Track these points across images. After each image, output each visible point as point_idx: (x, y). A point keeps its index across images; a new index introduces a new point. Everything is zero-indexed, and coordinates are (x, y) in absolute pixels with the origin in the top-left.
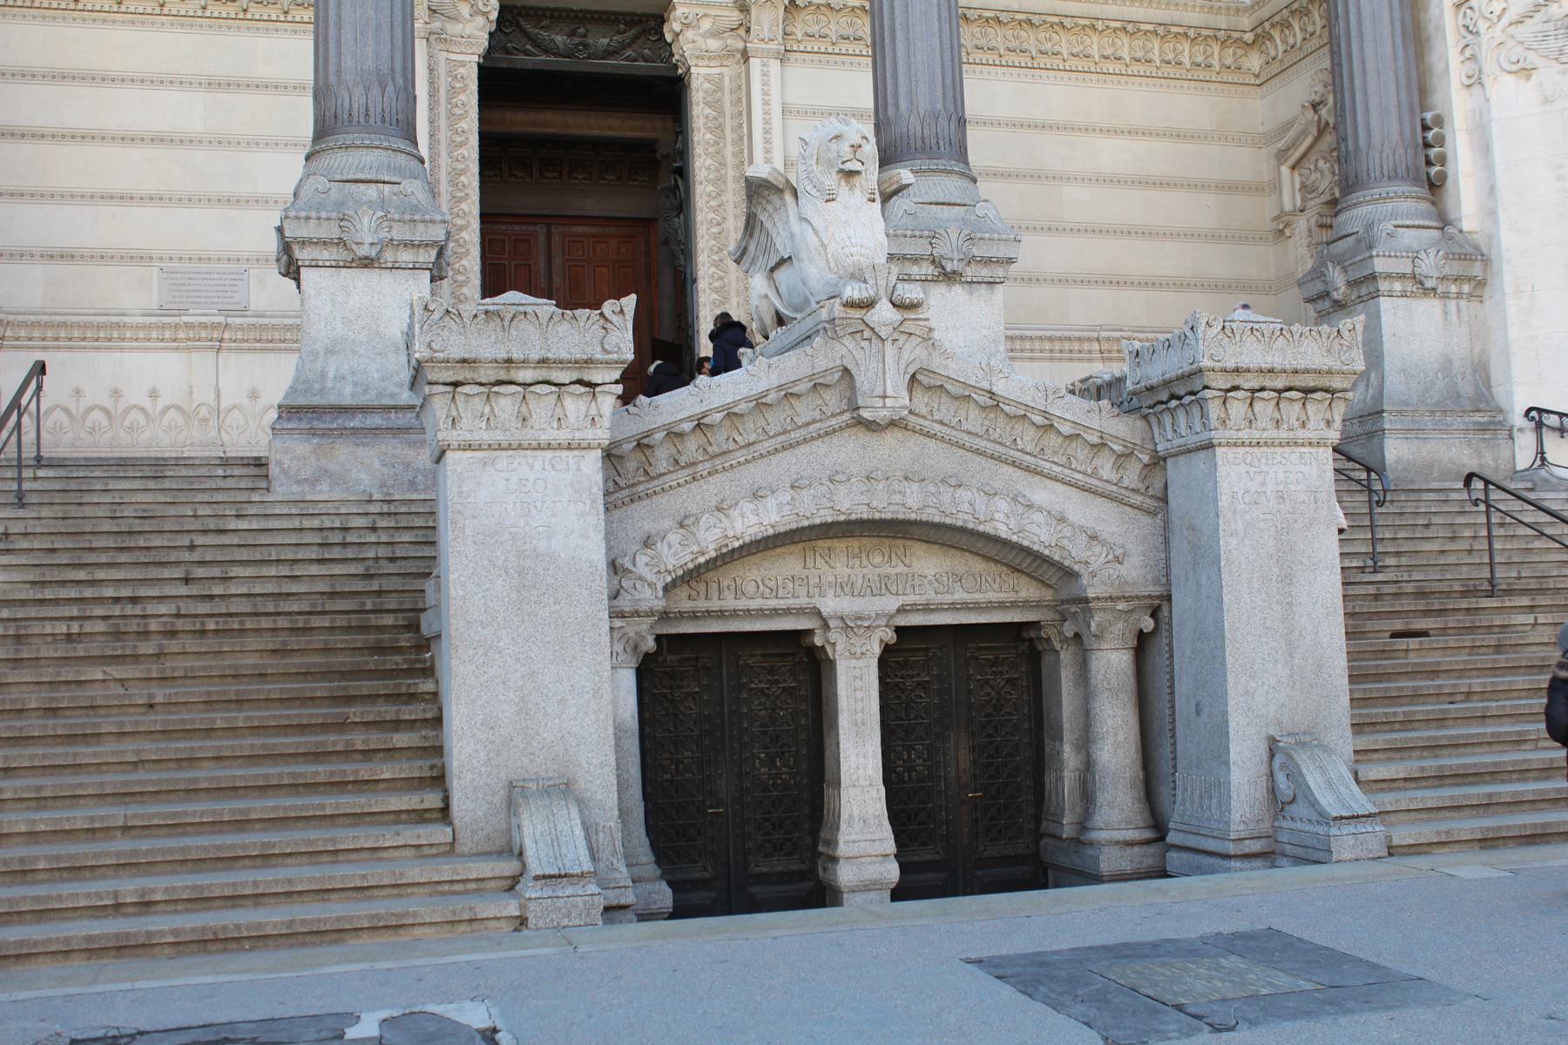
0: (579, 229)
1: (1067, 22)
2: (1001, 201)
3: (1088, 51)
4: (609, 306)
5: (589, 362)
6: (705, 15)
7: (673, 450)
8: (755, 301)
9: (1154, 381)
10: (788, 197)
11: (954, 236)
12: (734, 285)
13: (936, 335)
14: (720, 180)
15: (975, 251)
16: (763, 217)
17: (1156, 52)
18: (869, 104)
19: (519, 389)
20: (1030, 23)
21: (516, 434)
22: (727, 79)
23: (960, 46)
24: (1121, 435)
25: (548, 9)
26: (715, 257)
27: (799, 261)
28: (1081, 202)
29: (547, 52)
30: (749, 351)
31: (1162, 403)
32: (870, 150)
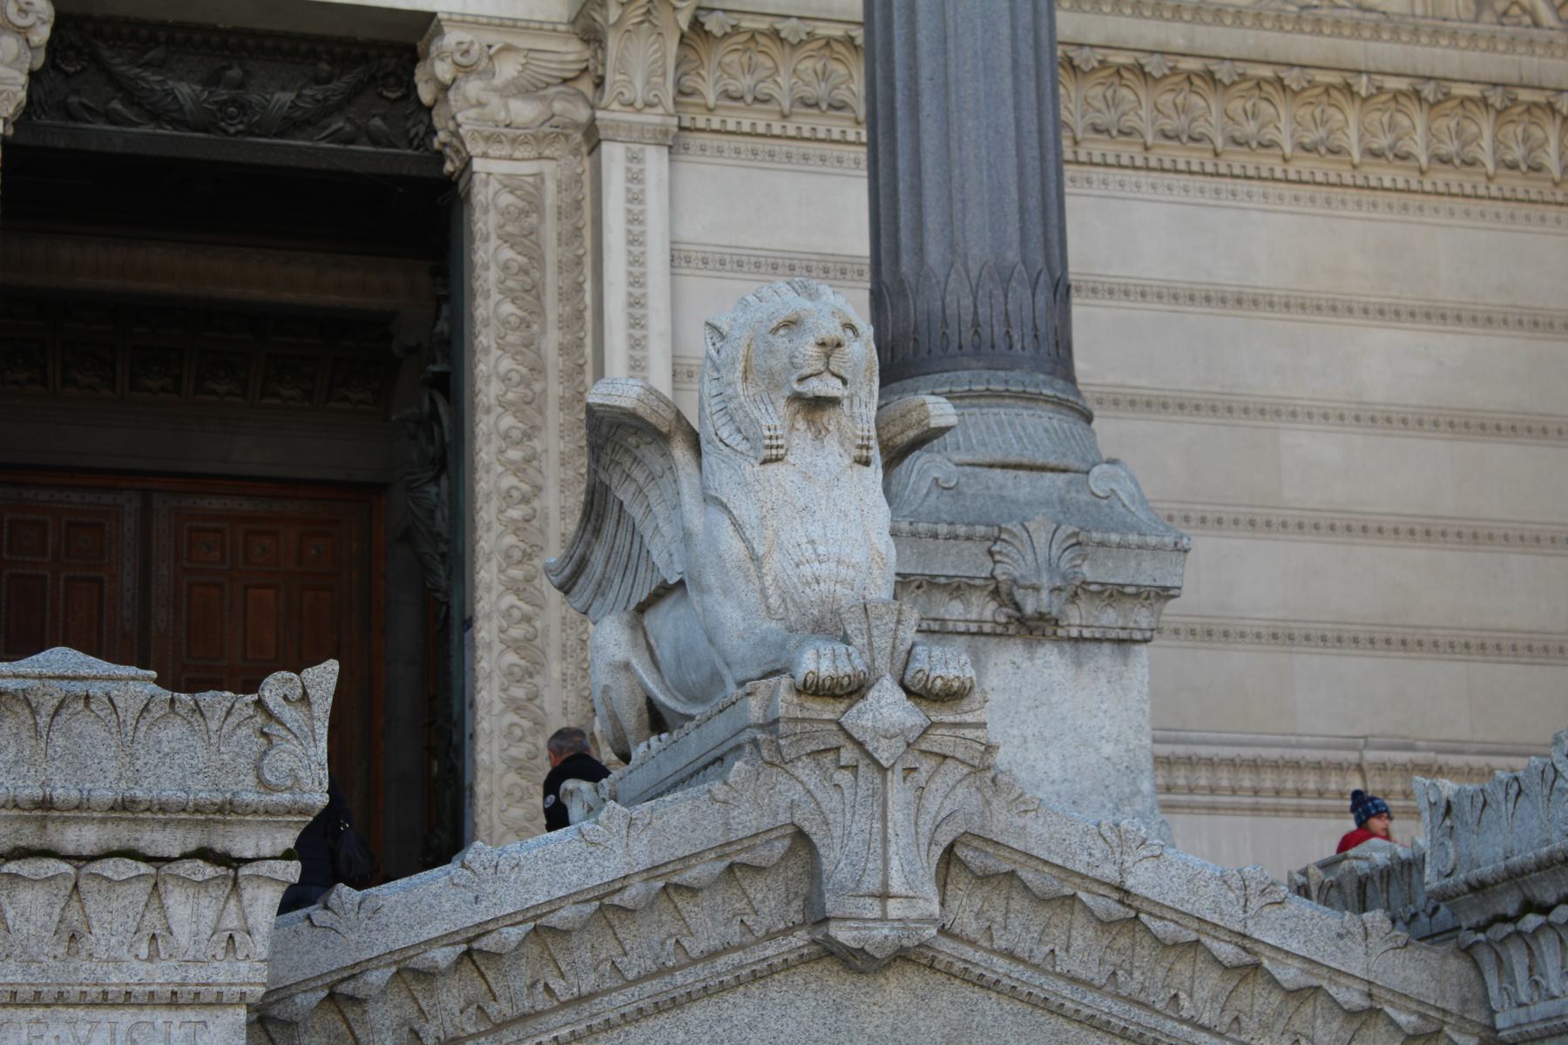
0: (215, 504)
1: (1292, 78)
2: (1144, 461)
3: (1339, 140)
4: (275, 687)
5: (227, 810)
6: (507, 49)
7: (410, 1010)
8: (601, 677)
9: (1487, 871)
10: (680, 452)
11: (1041, 539)
12: (555, 636)
13: (1001, 759)
14: (529, 406)
15: (1087, 571)
16: (624, 493)
17: (1486, 142)
18: (861, 246)
19: (65, 867)
20: (1210, 77)
21: (52, 971)
22: (550, 187)
23: (1059, 125)
24: (1413, 990)
25: (163, 25)
26: (516, 572)
27: (703, 590)
28: (1318, 466)
29: (156, 117)
30: (585, 786)
31: (1505, 919)
32: (862, 352)
